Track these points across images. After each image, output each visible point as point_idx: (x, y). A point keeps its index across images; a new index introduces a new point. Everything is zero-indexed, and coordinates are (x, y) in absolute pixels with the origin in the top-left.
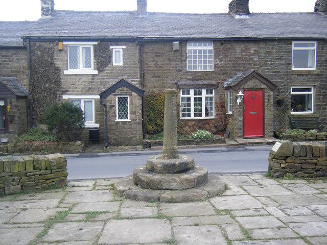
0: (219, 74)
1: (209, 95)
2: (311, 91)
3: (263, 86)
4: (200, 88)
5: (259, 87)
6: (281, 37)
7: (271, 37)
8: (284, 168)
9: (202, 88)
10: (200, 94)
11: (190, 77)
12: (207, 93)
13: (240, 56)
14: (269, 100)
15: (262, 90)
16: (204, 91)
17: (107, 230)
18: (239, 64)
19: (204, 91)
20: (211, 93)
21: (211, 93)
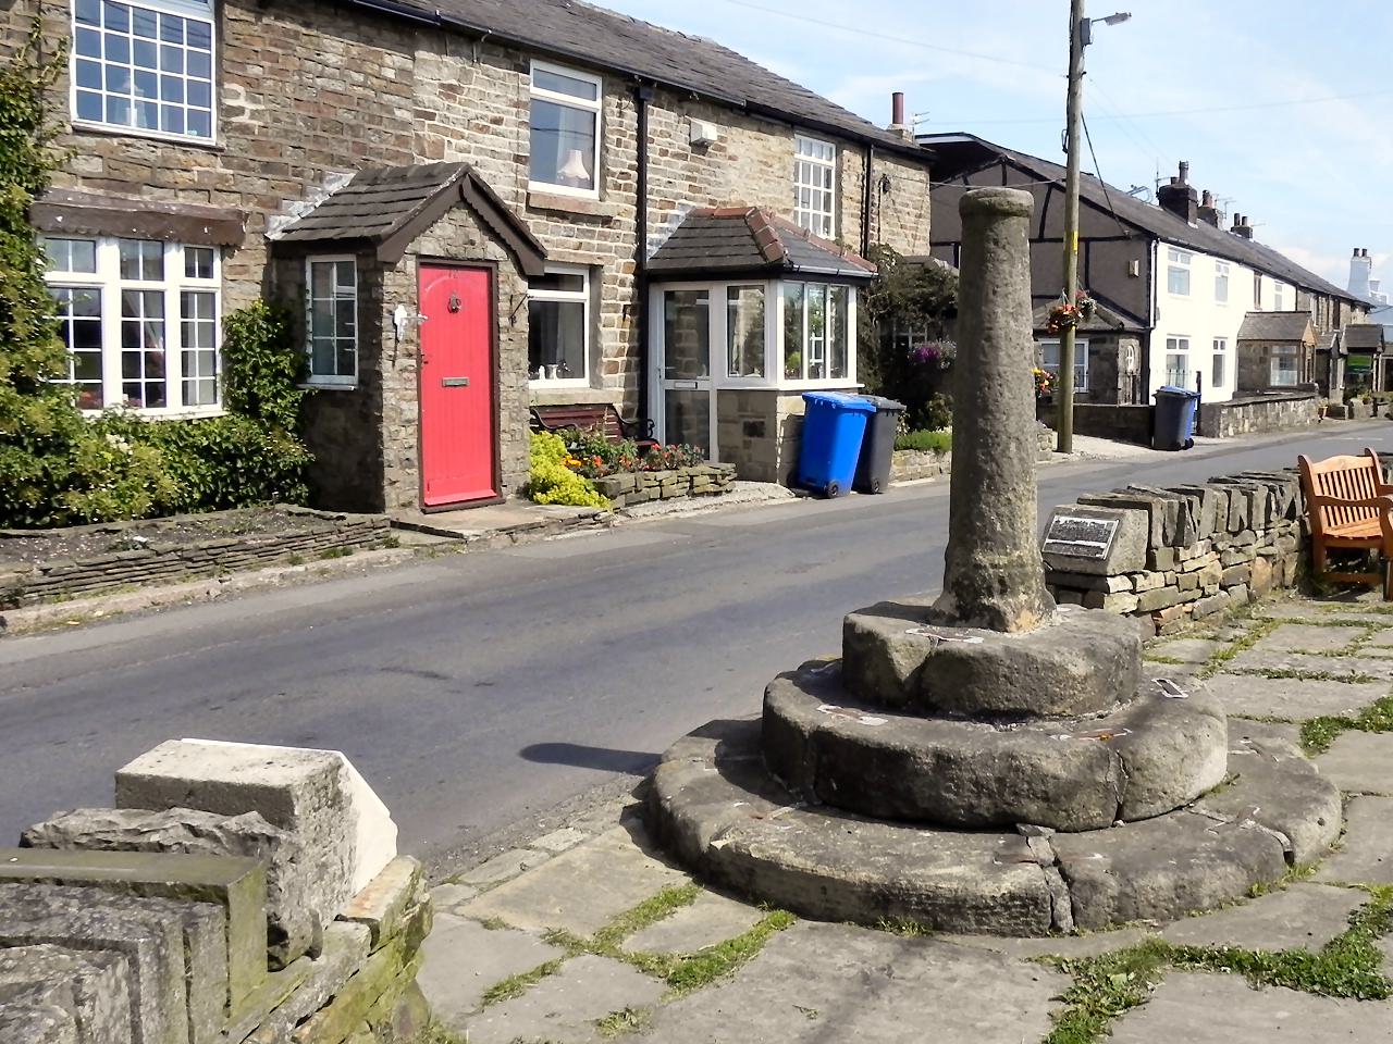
0: (243, 167)
1: (197, 283)
2: (737, 298)
3: (494, 251)
4: (998, 677)
5: (478, 253)
6: (744, 263)
7: (714, 268)
8: (1002, 925)
9: (162, 240)
10: (157, 270)
11: (95, 166)
12: (189, 272)
13: (339, 87)
14: (513, 319)
15: (488, 267)
16: (175, 258)
17: (1282, 992)
18: (340, 127)
19: (175, 258)
20: (206, 272)
21: (206, 272)
